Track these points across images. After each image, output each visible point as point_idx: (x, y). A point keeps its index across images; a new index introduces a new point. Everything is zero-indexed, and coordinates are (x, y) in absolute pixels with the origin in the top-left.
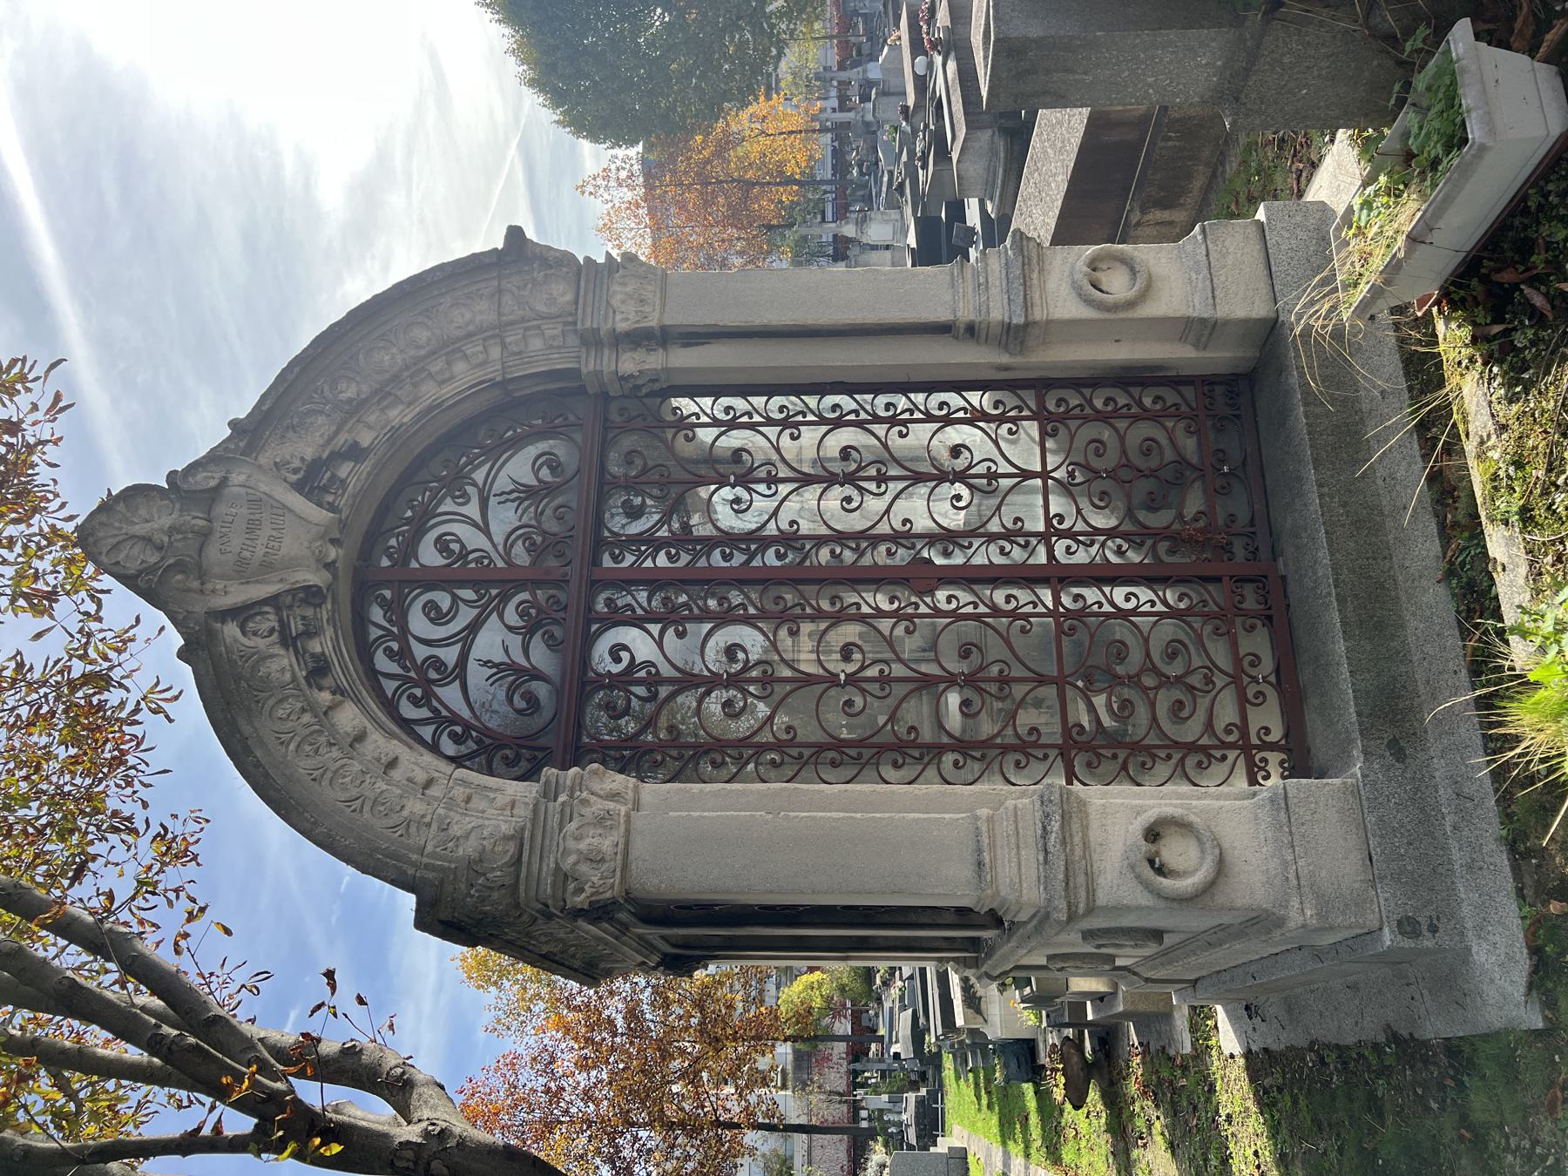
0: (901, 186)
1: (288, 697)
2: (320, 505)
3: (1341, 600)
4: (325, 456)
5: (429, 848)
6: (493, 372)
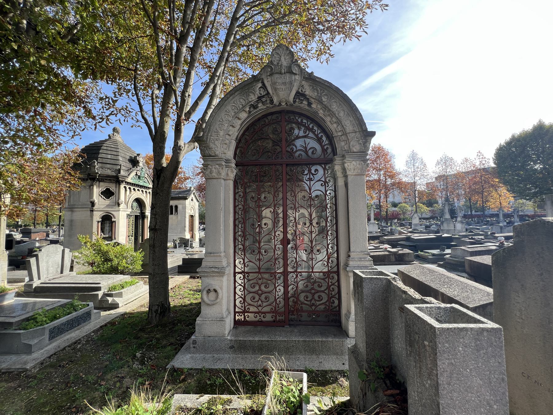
0: (472, 232)
2: (294, 98)
3: (268, 341)
5: (212, 137)
6: (335, 134)
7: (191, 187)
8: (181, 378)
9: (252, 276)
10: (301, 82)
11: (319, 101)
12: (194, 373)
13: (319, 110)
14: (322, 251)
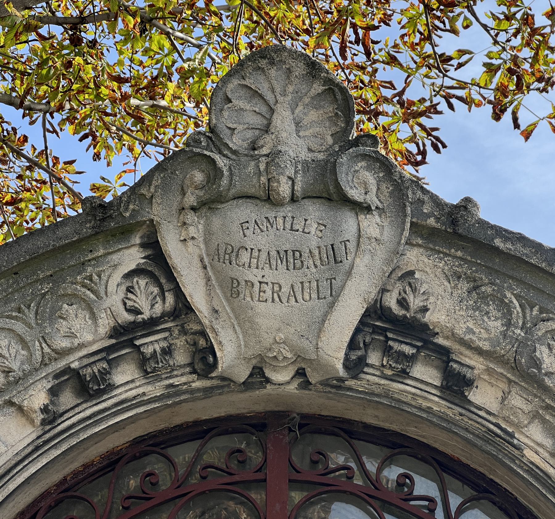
1: (28, 349)
2: (352, 345)
4: (440, 341)
10: (397, 253)
11: (515, 367)
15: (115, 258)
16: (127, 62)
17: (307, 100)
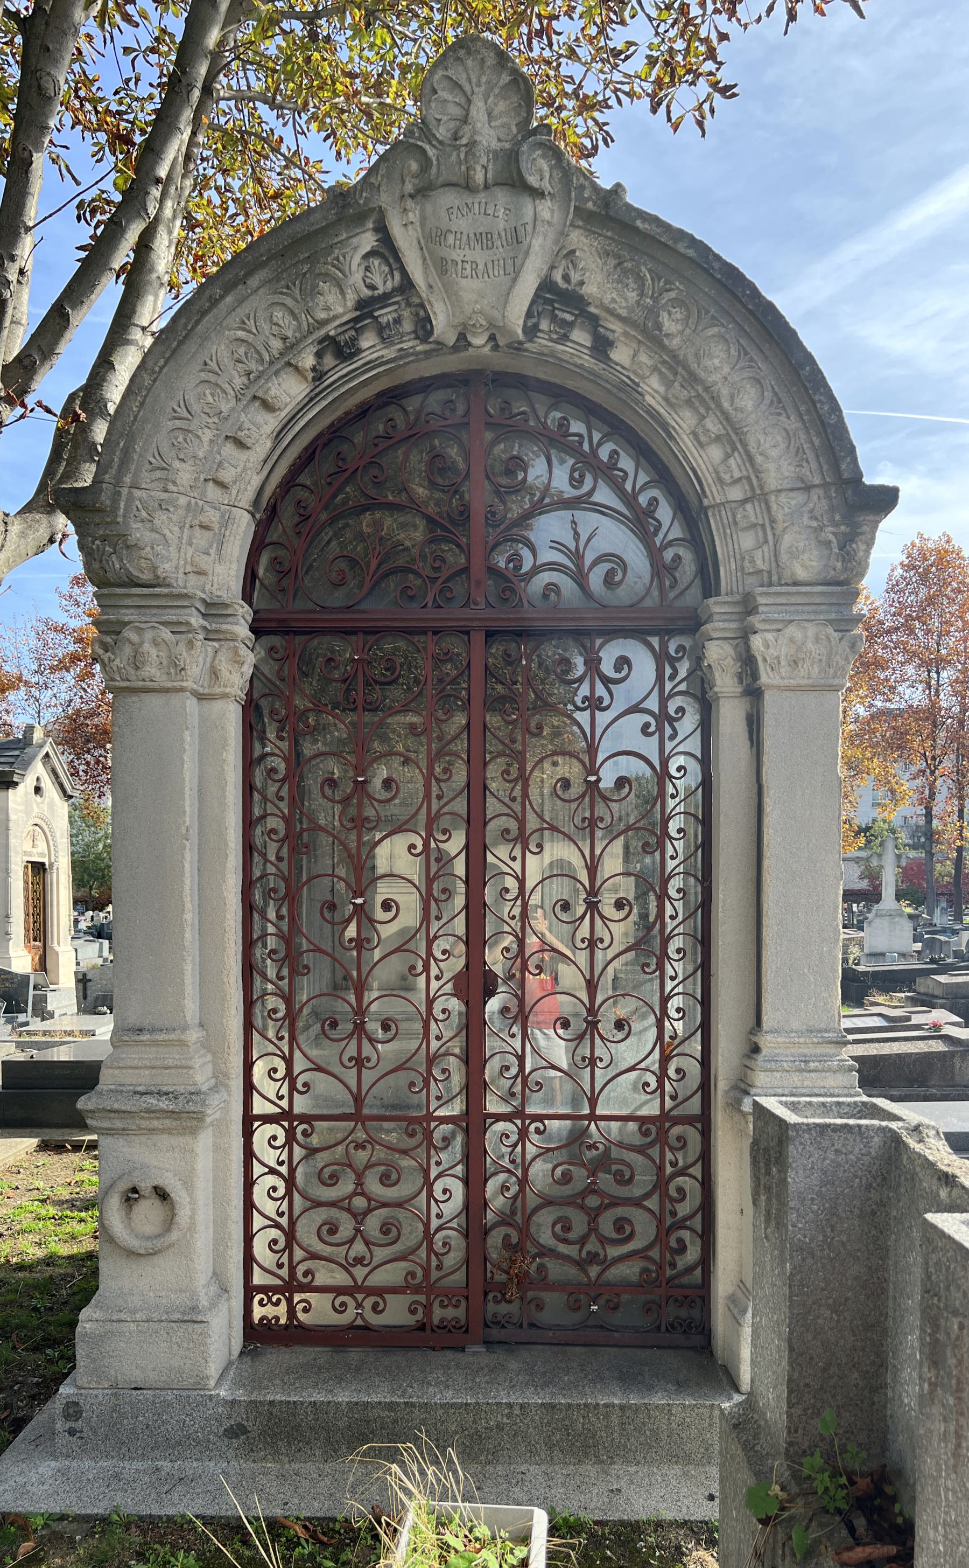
2: (529, 315)
3: (391, 1406)
4: (592, 309)
5: (137, 493)
6: (714, 495)
7: (30, 729)
8: (21, 1550)
9: (322, 1133)
10: (563, 234)
11: (644, 330)
12: (76, 1532)
13: (643, 378)
14: (636, 1027)
15: (355, 241)
16: (357, 60)
17: (497, 91)
